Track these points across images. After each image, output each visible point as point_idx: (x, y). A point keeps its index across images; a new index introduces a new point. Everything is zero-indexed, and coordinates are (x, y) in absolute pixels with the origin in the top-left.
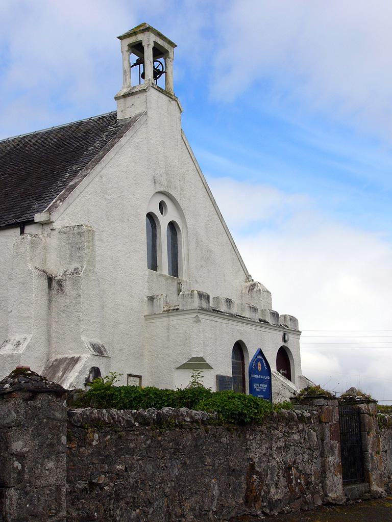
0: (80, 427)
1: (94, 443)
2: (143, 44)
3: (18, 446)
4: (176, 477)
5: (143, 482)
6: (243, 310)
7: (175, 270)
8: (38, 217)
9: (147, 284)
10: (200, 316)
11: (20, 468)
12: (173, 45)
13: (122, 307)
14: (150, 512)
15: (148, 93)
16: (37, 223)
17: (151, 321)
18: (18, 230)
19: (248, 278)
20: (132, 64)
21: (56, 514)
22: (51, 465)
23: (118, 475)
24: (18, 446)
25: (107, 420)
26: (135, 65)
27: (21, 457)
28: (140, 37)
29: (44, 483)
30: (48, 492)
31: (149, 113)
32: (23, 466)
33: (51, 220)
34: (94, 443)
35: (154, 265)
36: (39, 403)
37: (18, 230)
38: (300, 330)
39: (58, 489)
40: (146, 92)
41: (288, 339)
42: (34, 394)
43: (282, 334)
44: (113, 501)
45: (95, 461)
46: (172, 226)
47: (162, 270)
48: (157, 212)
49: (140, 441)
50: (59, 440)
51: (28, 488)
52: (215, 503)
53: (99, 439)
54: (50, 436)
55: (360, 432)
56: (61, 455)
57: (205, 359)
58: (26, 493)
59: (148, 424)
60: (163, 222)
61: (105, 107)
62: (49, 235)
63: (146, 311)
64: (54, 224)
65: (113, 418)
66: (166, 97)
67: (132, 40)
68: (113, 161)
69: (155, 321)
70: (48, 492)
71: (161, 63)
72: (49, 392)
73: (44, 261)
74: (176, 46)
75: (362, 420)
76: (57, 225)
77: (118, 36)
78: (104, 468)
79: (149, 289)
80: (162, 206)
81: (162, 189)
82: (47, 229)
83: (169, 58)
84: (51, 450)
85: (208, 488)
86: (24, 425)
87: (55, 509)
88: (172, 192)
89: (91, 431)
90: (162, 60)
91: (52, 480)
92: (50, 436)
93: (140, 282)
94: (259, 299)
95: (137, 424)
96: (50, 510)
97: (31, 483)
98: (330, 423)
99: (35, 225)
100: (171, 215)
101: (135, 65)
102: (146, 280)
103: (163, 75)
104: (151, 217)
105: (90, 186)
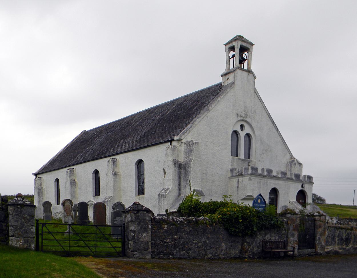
0: (159, 223)
1: (165, 228)
2: (235, 47)
3: (132, 228)
4: (203, 241)
5: (187, 242)
6: (278, 174)
7: (248, 155)
8: (176, 138)
9: (231, 163)
10: (251, 177)
11: (133, 235)
12: (253, 45)
13: (217, 174)
14: (190, 253)
15: (236, 72)
16: (175, 140)
17: (232, 179)
18: (169, 144)
19: (292, 155)
20: (230, 58)
21: (147, 250)
22: (145, 234)
23: (176, 239)
24: (132, 228)
25: (171, 221)
26: (232, 58)
27: (134, 231)
28: (234, 44)
29: (142, 240)
30: (144, 243)
31: (236, 83)
32: (134, 235)
33: (181, 139)
34: (165, 228)
35: (236, 153)
36: (140, 214)
37: (169, 144)
38: (313, 182)
39: (148, 242)
40: (234, 72)
41: (305, 186)
42: (138, 211)
43: (302, 184)
44: (173, 248)
45: (165, 234)
46: (248, 135)
47: (240, 156)
48: (238, 129)
49: (188, 228)
50: (148, 227)
51: (137, 241)
52: (223, 252)
53: (167, 227)
54: (144, 225)
55: (314, 228)
56: (149, 232)
57: (253, 196)
58: (136, 243)
59: (191, 223)
60: (242, 134)
61: (218, 80)
62: (180, 145)
63: (230, 175)
64: (182, 141)
65: (174, 220)
66: (51, 173)
67: (230, 45)
68: (214, 108)
69: (233, 179)
70: (144, 243)
71: (246, 55)
72: (143, 210)
73: (178, 156)
74: (254, 45)
75: (316, 223)
76: (184, 141)
77: (224, 44)
78: (169, 237)
79: (232, 165)
80: (242, 127)
81: (242, 119)
82: (180, 143)
83: (250, 52)
84: (145, 230)
85: (220, 246)
86: (134, 222)
87: (147, 248)
88: (247, 119)
89: (164, 224)
90: (246, 53)
91: (146, 239)
92: (144, 225)
93: (227, 162)
94: (295, 167)
95: (185, 222)
96: (145, 248)
97: (138, 240)
98: (293, 224)
99: (176, 141)
100: (247, 130)
101: (232, 58)
102: (230, 161)
103: (247, 61)
104: (235, 132)
105: (201, 122)
